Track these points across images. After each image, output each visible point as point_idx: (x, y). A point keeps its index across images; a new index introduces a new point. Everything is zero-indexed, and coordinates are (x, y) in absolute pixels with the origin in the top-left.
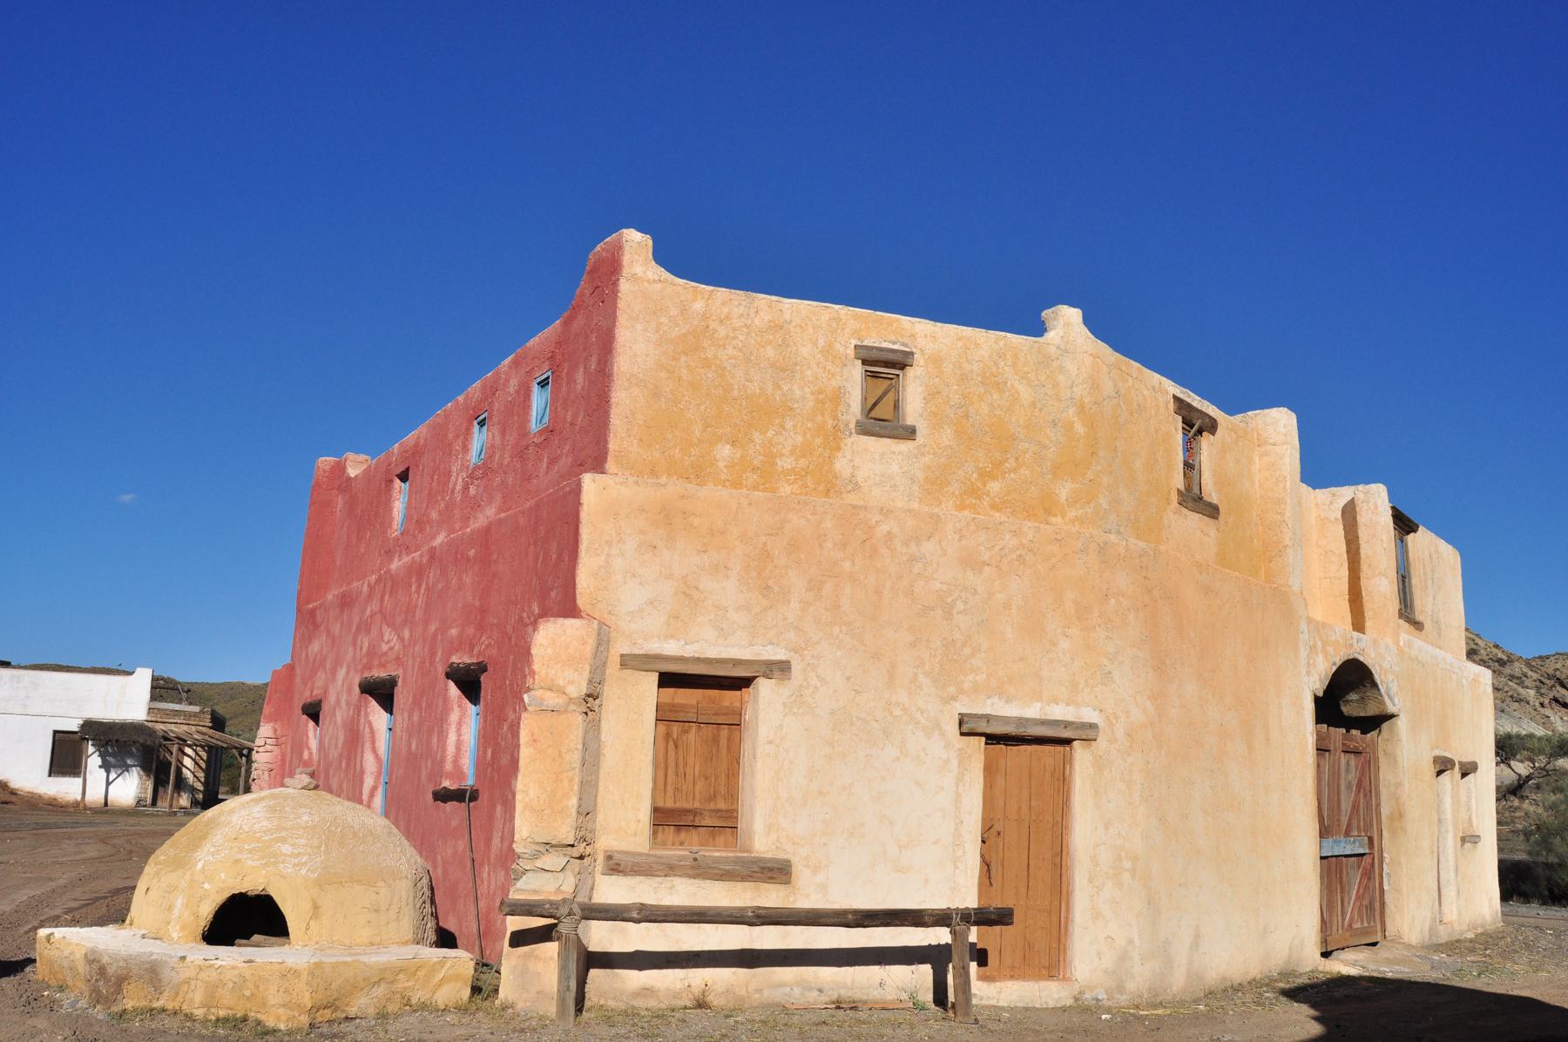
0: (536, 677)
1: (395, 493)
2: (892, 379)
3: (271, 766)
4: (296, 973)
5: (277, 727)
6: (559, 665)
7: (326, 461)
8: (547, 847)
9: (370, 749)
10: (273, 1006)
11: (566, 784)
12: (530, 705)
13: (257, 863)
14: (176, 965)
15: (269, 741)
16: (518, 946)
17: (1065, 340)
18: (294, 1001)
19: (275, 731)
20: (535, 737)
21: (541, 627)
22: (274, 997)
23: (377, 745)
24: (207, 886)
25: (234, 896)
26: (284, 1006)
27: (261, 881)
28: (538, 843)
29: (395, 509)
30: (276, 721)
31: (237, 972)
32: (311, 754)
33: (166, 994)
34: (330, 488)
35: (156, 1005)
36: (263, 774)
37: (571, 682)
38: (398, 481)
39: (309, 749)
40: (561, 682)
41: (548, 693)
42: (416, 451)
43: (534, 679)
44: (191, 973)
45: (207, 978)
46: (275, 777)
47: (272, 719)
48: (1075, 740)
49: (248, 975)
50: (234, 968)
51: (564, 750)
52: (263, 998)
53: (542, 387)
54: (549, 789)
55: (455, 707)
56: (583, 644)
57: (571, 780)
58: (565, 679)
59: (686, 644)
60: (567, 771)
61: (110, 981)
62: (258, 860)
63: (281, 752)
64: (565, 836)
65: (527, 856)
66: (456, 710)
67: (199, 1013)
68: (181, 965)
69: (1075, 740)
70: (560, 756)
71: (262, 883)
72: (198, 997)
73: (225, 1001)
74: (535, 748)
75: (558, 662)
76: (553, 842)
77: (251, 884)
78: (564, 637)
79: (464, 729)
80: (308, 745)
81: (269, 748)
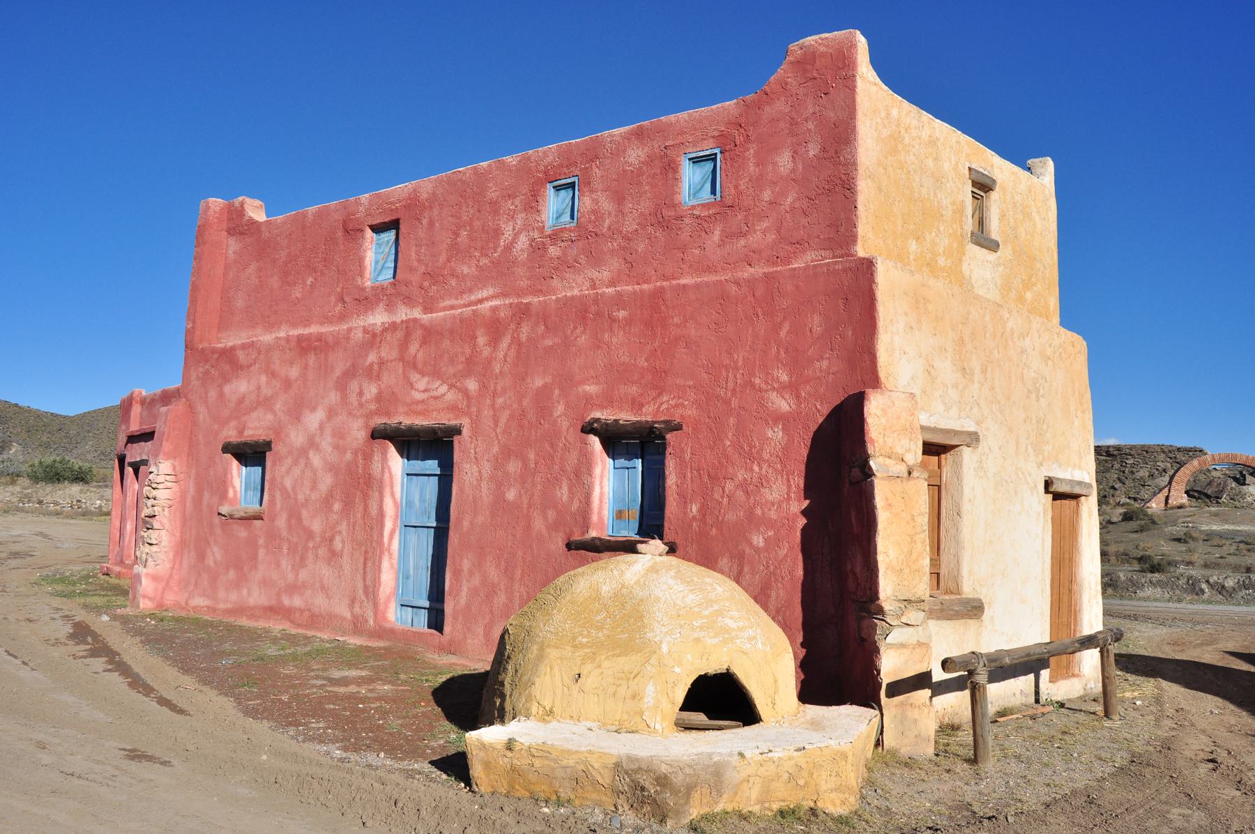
0: (876, 444)
1: (367, 244)
2: (978, 199)
3: (170, 502)
4: (844, 756)
5: (176, 464)
6: (895, 435)
7: (216, 202)
8: (905, 603)
9: (389, 493)
10: (825, 791)
11: (919, 545)
12: (878, 471)
13: (715, 641)
14: (737, 764)
15: (168, 478)
16: (893, 696)
17: (940, 182)
18: (844, 784)
19: (174, 468)
20: (890, 502)
21: (872, 398)
22: (825, 782)
23: (395, 489)
24: (677, 670)
25: (700, 677)
26: (835, 790)
27: (725, 659)
28: (899, 600)
29: (368, 259)
30: (175, 458)
31: (792, 762)
32: (235, 492)
33: (725, 796)
34: (219, 229)
35: (718, 809)
36: (163, 510)
37: (909, 451)
38: (370, 231)
39: (234, 487)
40: (900, 451)
41: (888, 461)
42: (414, 204)
43: (874, 447)
44: (750, 770)
45: (766, 773)
46: (175, 514)
47: (169, 456)
48: (1083, 495)
49: (802, 762)
50: (790, 758)
51: (915, 514)
52: (816, 785)
53: (693, 162)
54: (905, 550)
55: (599, 460)
56: (911, 415)
57: (923, 542)
58: (902, 448)
59: (930, 416)
60: (920, 533)
61: (680, 792)
62: (714, 637)
63: (180, 488)
64: (923, 593)
65: (891, 612)
66: (600, 463)
67: (756, 809)
68: (742, 763)
69: (1083, 495)
70: (913, 519)
71: (726, 661)
72: (755, 794)
73: (778, 794)
74: (890, 512)
75: (894, 432)
76: (913, 599)
77: (714, 666)
78: (894, 409)
79: (605, 482)
80: (232, 483)
81: (169, 485)
